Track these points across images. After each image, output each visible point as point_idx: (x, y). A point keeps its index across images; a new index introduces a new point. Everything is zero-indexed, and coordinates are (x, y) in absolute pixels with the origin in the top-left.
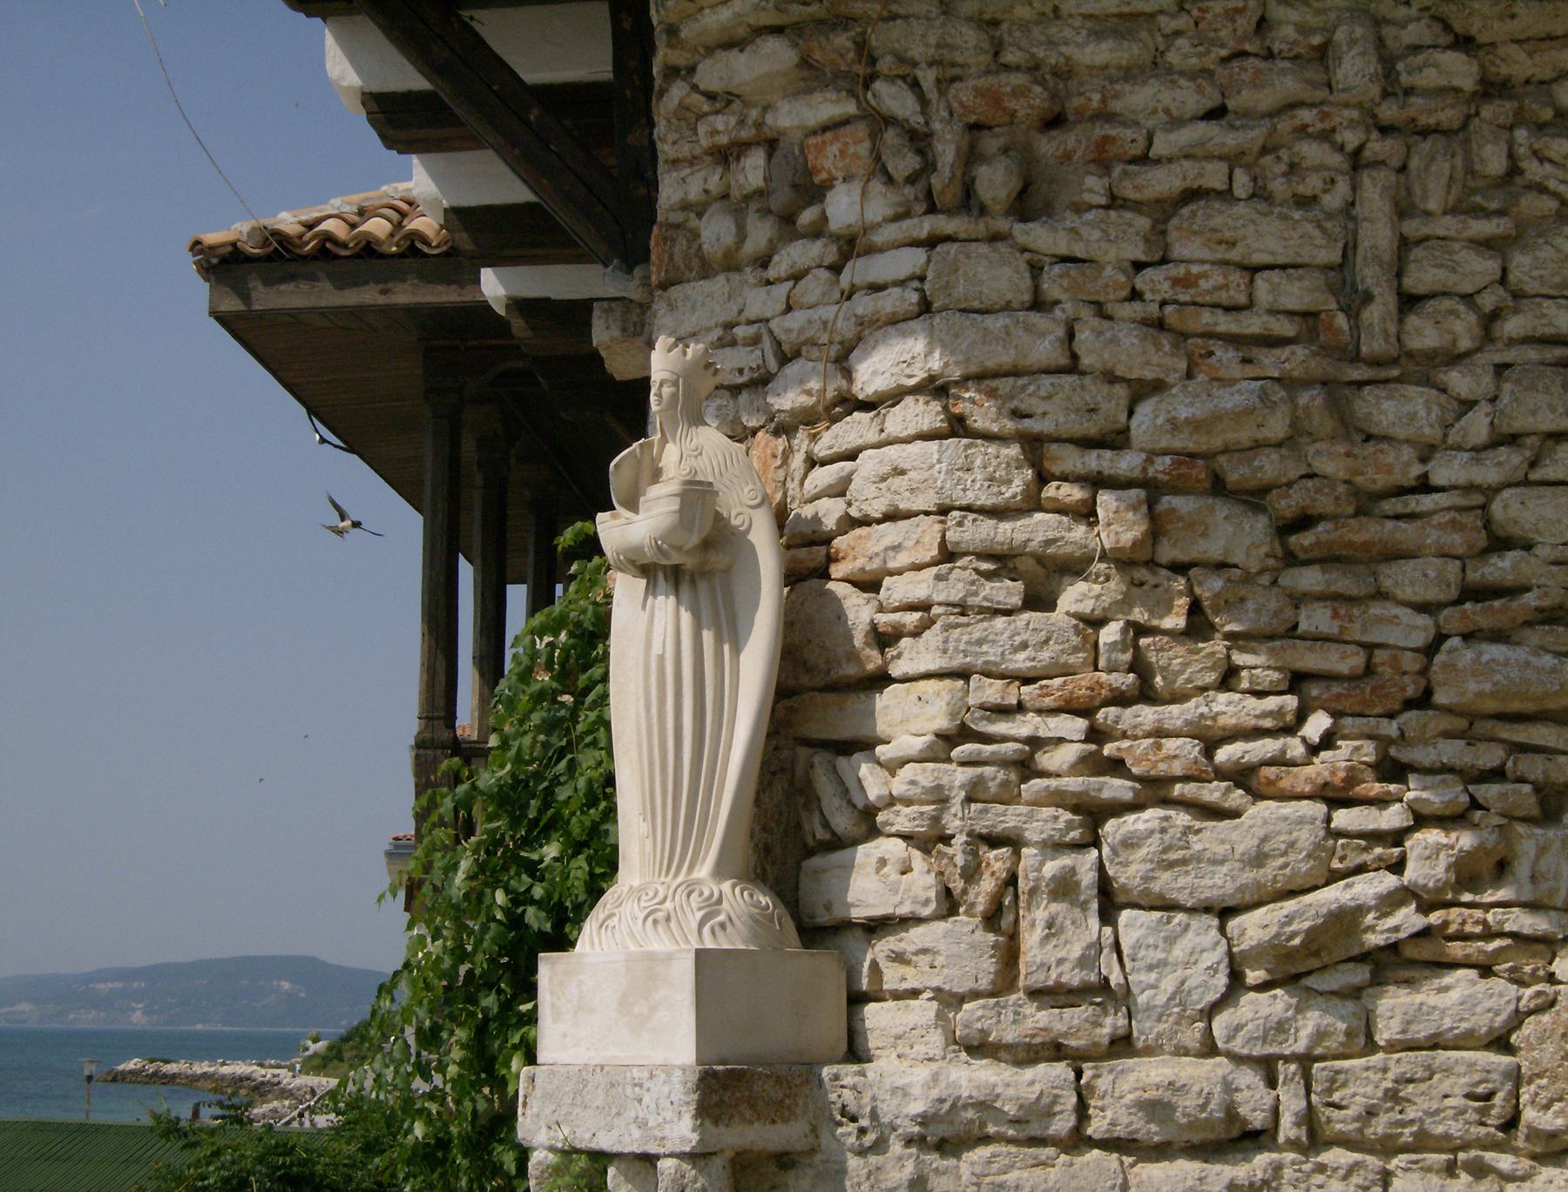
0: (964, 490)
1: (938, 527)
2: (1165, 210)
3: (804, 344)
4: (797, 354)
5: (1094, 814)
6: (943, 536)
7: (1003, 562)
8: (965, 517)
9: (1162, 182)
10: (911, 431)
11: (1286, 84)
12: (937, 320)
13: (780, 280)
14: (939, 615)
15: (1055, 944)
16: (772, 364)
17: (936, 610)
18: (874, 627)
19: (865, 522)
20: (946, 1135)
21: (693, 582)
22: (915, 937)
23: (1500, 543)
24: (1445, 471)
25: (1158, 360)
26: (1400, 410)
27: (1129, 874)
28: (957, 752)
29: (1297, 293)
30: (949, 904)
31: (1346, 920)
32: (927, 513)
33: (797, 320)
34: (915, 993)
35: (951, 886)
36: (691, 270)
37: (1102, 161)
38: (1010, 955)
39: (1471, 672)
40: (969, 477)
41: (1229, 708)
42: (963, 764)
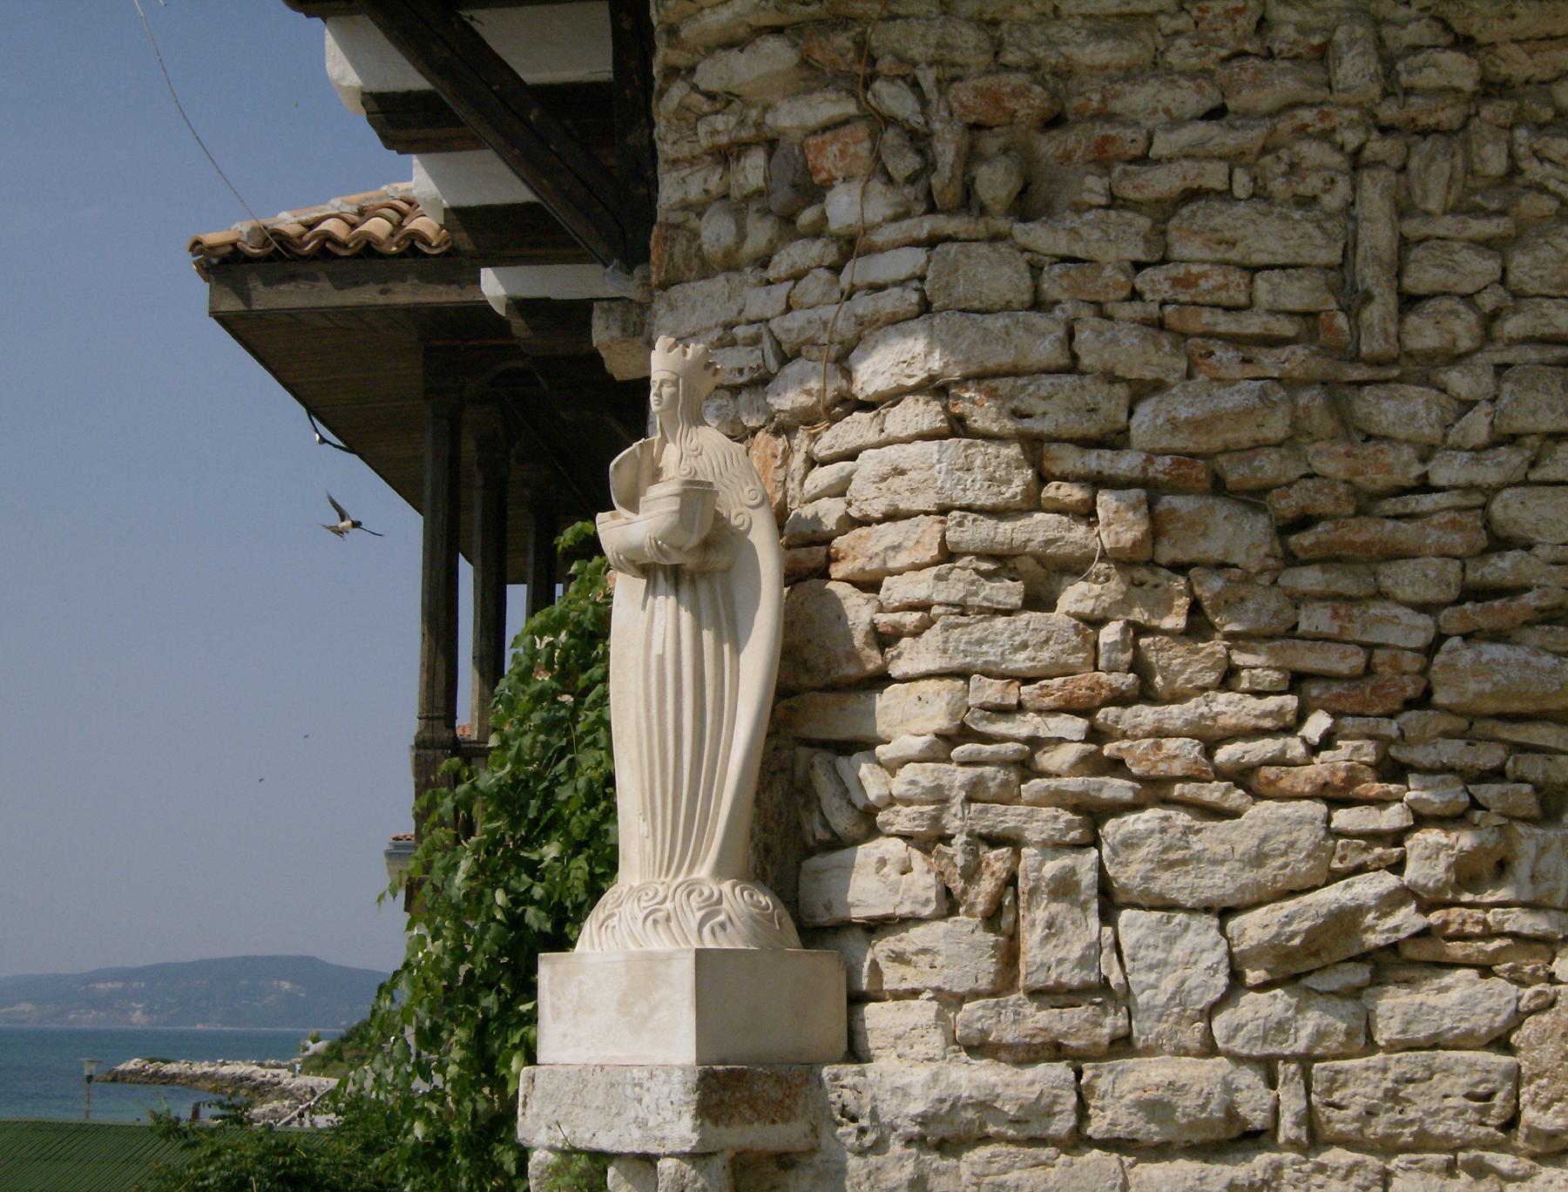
0: (964, 490)
1: (938, 527)
2: (1165, 210)
3: (804, 344)
4: (797, 354)
5: (1094, 814)
6: (943, 536)
7: (1003, 562)
8: (965, 517)
9: (1162, 182)
10: (911, 431)
11: (1286, 84)
12: (937, 320)
13: (780, 280)
14: (939, 615)
15: (1055, 944)
16: (772, 364)
17: (936, 610)
18: (874, 627)
19: (865, 522)
20: (946, 1135)
21: (693, 582)
22: (915, 937)
23: (1500, 543)
24: (1445, 471)
25: (1158, 360)
26: (1400, 410)
27: (1129, 874)
28: (957, 752)
29: (1297, 293)
30: (949, 904)
31: (1346, 920)
32: (927, 513)
33: (797, 320)
34: (915, 993)
35: (951, 886)
36: (691, 270)
37: (1102, 161)
38: (1010, 955)
39: (1471, 672)
40: (969, 477)
41: (1229, 708)
42: (963, 764)
